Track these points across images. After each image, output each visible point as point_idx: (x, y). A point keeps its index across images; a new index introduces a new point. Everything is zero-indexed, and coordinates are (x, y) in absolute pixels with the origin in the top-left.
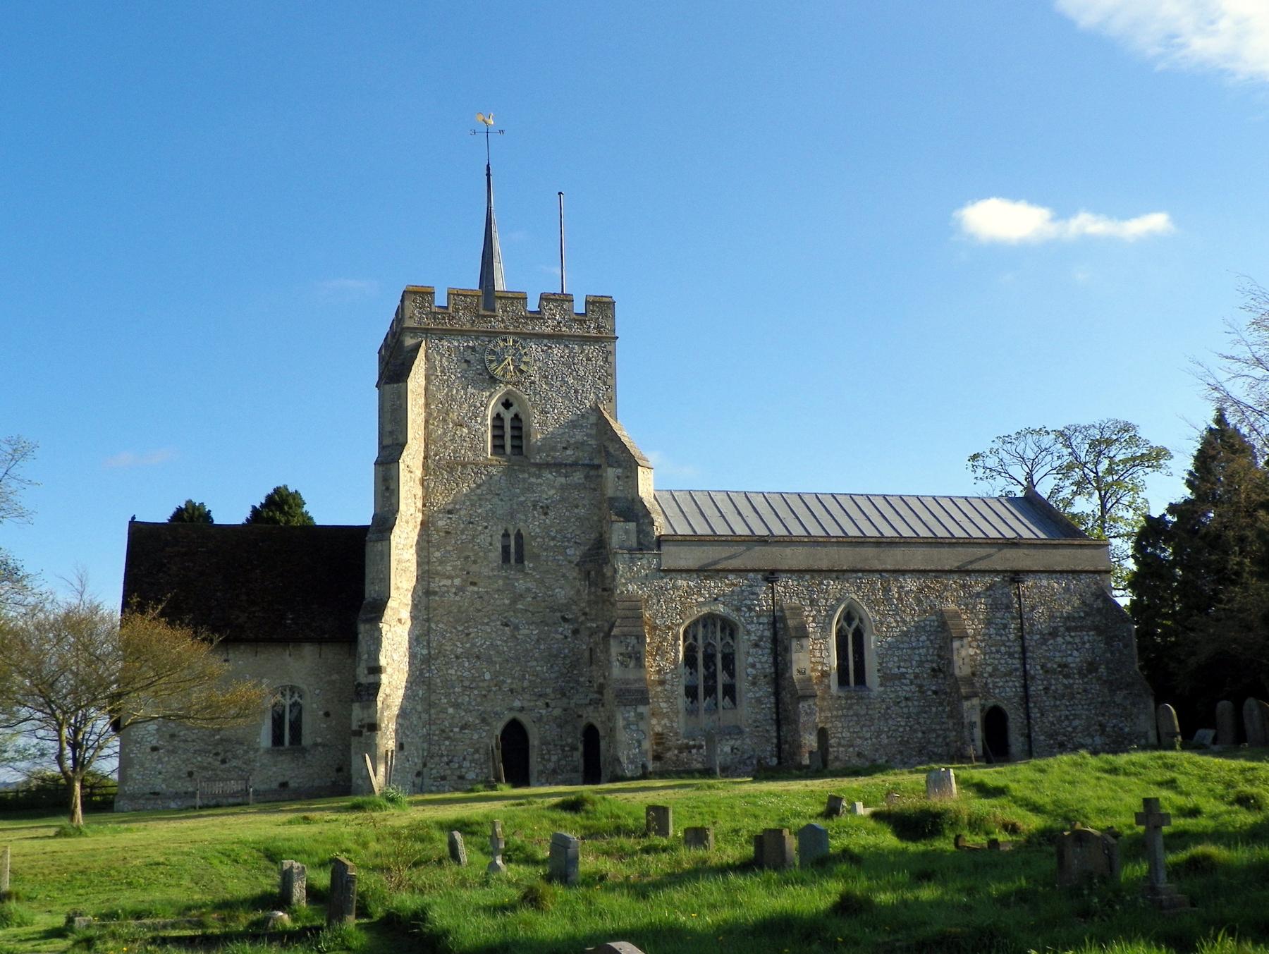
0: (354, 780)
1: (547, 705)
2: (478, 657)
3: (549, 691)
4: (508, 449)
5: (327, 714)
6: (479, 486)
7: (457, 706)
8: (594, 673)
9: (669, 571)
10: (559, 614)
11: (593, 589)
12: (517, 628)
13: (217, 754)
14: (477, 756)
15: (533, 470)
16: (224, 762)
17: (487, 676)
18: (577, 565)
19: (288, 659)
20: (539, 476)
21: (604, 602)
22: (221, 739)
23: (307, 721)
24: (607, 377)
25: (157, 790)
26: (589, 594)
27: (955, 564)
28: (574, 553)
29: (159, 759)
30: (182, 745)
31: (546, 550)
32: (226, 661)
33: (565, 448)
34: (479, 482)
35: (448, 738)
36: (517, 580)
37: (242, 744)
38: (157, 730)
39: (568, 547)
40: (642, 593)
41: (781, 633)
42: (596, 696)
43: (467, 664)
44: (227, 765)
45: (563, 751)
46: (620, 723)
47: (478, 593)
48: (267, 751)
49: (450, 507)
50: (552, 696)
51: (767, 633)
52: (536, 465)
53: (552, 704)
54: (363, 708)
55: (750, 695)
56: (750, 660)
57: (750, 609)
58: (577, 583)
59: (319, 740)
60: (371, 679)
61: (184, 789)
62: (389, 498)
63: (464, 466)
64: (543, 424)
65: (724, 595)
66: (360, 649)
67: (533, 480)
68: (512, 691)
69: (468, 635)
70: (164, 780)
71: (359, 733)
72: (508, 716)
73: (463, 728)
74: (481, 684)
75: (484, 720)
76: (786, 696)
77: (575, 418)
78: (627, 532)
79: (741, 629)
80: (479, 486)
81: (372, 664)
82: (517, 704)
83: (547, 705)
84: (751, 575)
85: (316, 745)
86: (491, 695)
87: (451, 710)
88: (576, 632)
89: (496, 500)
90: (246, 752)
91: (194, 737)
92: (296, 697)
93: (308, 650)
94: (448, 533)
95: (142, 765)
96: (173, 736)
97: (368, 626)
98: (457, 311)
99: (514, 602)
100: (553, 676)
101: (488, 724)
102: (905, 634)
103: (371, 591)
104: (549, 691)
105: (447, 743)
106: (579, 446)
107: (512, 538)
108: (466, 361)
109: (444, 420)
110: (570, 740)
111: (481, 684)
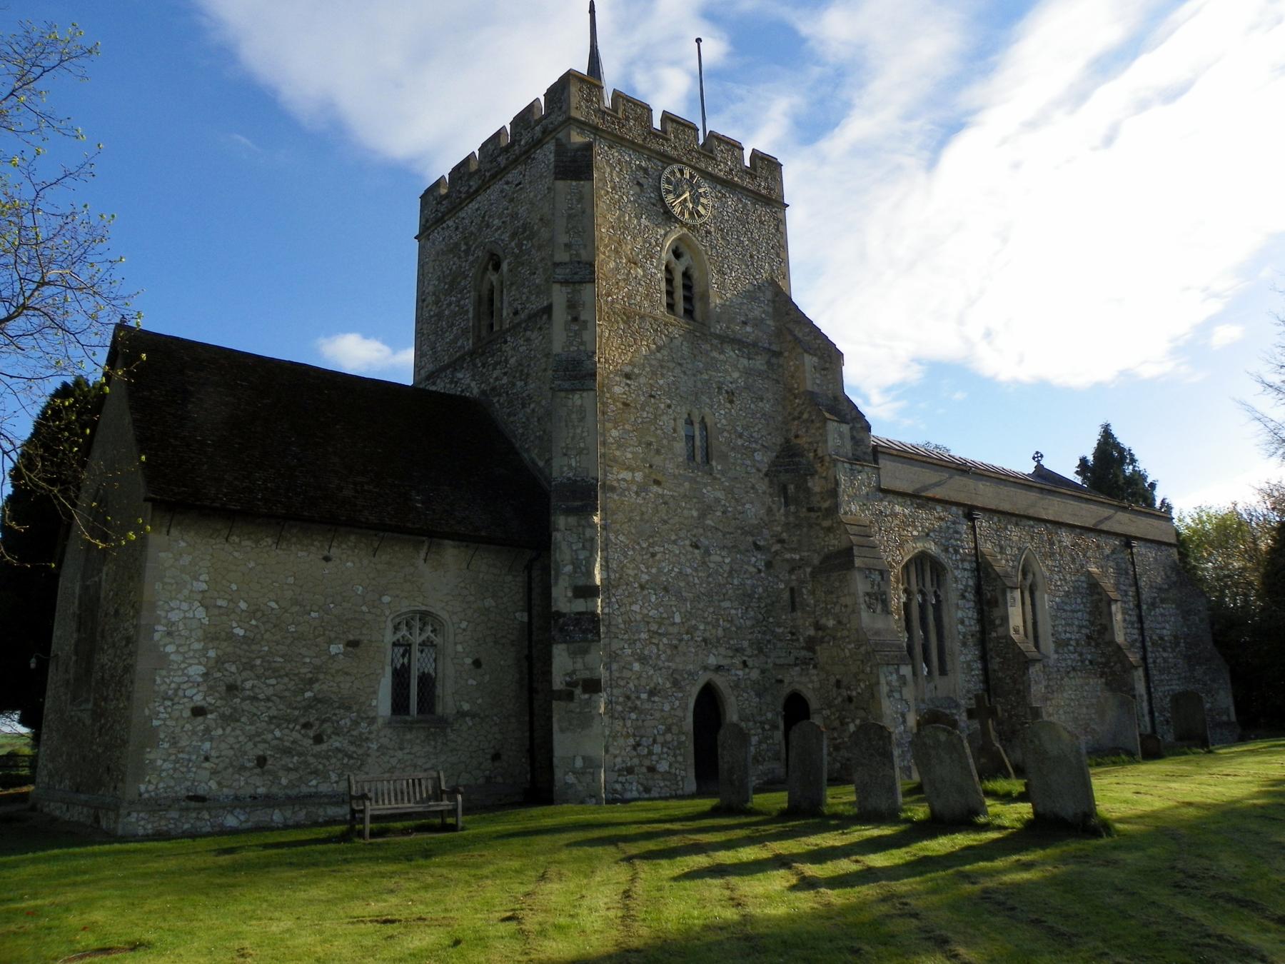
0: (558, 774)
1: (745, 664)
2: (666, 589)
3: (745, 644)
5: (477, 663)
6: (659, 349)
7: (643, 659)
8: (800, 622)
9: (886, 492)
10: (750, 539)
11: (792, 508)
12: (707, 552)
13: (307, 726)
14: (669, 737)
15: (715, 342)
16: (318, 739)
17: (677, 619)
18: (766, 475)
20: (722, 352)
21: (810, 526)
22: (315, 698)
25: (201, 792)
26: (786, 515)
27: (1089, 523)
28: (763, 459)
29: (207, 730)
30: (246, 705)
31: (733, 449)
32: (327, 559)
33: (745, 323)
34: (660, 343)
35: (634, 709)
36: (705, 485)
37: (349, 708)
38: (205, 675)
39: (755, 450)
40: (866, 517)
41: (987, 589)
42: (804, 653)
43: (653, 598)
44: (324, 747)
45: (763, 729)
46: (884, 689)
47: (663, 496)
48: (389, 724)
49: (628, 369)
50: (749, 652)
51: (971, 583)
52: (718, 337)
53: (750, 663)
54: (573, 654)
55: (962, 658)
56: (960, 614)
57: (956, 552)
58: (768, 500)
59: (466, 707)
60: (580, 606)
61: (250, 791)
62: (578, 334)
63: (642, 317)
64: (722, 286)
65: (934, 531)
66: (557, 556)
67: (715, 354)
68: (705, 640)
69: (653, 555)
70: (214, 772)
71: (569, 696)
72: (703, 679)
73: (652, 693)
74: (671, 629)
75: (676, 683)
76: (995, 663)
77: (751, 288)
78: (841, 435)
79: (949, 576)
80: (659, 349)
81: (581, 582)
82: (712, 660)
83: (745, 664)
84: (954, 509)
85: (462, 714)
86: (682, 647)
87: (637, 666)
88: (769, 565)
89: (678, 371)
90: (356, 723)
91: (270, 691)
92: (428, 632)
93: (451, 554)
94: (626, 405)
95: (174, 743)
96: (232, 688)
97: (572, 520)
98: (627, 119)
99: (703, 516)
100: (749, 623)
101: (681, 689)
102: (1067, 594)
104: (745, 644)
105: (633, 716)
106: (758, 323)
107: (697, 426)
108: (639, 184)
109: (617, 251)
110: (769, 715)
111: (671, 629)
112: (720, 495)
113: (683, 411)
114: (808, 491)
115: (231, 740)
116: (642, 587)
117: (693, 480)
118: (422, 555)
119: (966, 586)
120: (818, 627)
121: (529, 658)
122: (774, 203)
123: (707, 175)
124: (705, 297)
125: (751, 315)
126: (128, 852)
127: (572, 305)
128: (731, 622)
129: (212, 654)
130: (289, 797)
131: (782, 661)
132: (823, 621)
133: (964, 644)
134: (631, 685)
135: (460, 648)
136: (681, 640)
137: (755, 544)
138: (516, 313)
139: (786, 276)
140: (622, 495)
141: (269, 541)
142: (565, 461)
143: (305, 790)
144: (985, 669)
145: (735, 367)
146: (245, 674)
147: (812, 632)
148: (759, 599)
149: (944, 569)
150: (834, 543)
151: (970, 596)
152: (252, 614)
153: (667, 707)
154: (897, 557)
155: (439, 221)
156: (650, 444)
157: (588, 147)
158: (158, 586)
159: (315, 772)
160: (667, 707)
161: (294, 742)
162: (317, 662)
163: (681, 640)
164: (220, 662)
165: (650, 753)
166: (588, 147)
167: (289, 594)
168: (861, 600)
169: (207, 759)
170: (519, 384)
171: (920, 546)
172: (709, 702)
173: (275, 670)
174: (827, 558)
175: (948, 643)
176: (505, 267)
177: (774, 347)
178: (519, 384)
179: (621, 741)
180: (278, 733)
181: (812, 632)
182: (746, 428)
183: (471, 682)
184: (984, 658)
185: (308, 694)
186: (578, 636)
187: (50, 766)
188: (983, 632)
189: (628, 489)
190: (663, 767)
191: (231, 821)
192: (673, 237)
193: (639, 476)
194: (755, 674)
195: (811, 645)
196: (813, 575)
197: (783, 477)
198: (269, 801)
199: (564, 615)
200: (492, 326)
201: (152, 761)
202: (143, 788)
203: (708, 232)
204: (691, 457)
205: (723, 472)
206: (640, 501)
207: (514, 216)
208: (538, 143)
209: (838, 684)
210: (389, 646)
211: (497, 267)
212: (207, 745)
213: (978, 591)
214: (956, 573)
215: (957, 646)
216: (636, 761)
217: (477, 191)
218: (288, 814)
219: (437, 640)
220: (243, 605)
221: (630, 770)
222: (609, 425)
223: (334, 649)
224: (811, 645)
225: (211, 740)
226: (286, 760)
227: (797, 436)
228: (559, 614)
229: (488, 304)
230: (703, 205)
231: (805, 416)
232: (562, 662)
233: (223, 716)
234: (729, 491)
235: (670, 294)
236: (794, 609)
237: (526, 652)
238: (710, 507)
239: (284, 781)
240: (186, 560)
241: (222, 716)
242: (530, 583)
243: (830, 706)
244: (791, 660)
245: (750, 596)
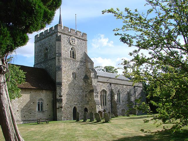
0: (58, 117)
4: (72, 57)
5: (47, 105)
9: (99, 82)
16: (30, 114)
19: (41, 93)
23: (44, 105)
24: (86, 47)
28: (83, 77)
41: (112, 95)
46: (97, 108)
48: (38, 112)
60: (60, 98)
71: (59, 109)
75: (71, 107)
76: (113, 104)
82: (75, 104)
88: (83, 91)
93: (44, 91)
103: (57, 81)
113: (72, 71)
120: (89, 99)
121: (53, 104)
123: (76, 37)
124: (75, 55)
127: (58, 59)
142: (58, 80)
143: (29, 119)
150: (91, 89)
154: (99, 90)
155: (38, 41)
157: (60, 36)
159: (30, 117)
166: (60, 36)
171: (103, 89)
172: (75, 109)
174: (91, 90)
176: (48, 50)
177: (85, 62)
184: (111, 103)
188: (111, 100)
190: (69, 117)
192: (71, 47)
194: (81, 105)
195: (88, 102)
200: (46, 58)
203: (76, 46)
207: (50, 44)
208: (53, 34)
211: (47, 50)
213: (111, 94)
217: (44, 38)
219: (43, 102)
223: (31, 103)
224: (88, 102)
226: (27, 116)
229: (46, 55)
232: (58, 105)
235: (71, 55)
242: (53, 95)
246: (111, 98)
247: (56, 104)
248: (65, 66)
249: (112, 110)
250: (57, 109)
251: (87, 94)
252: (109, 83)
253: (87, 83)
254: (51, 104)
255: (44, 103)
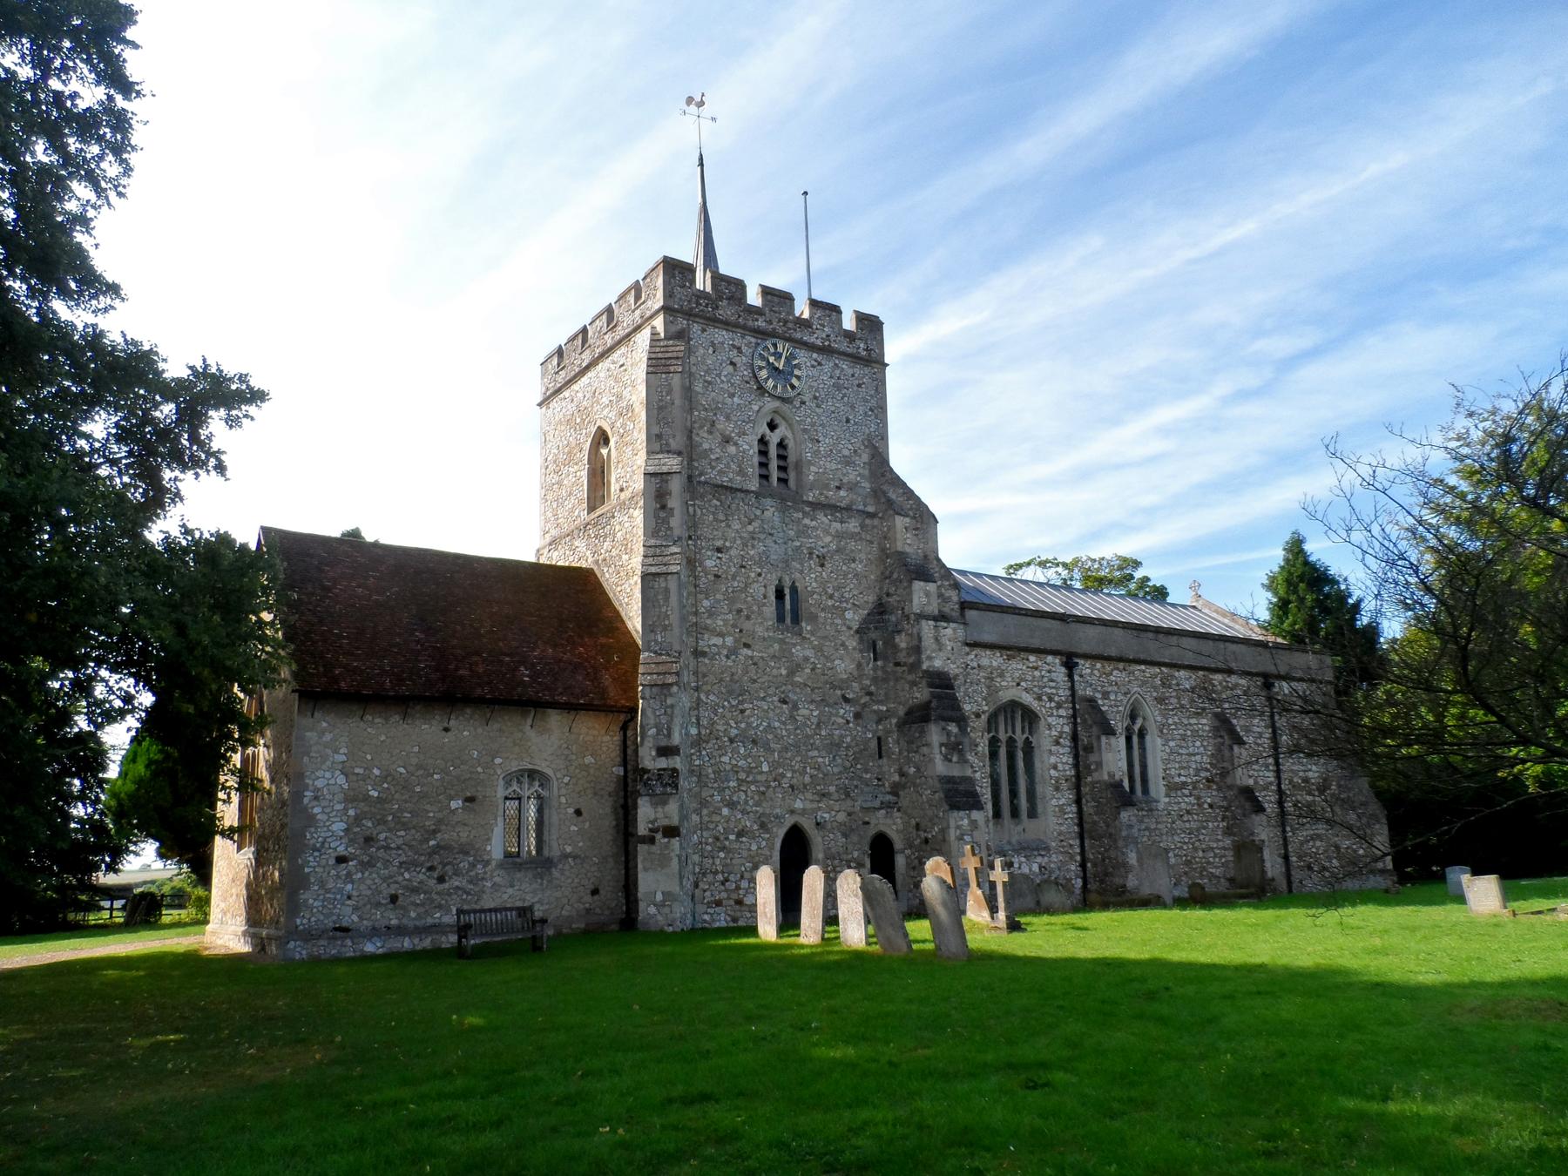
0: (642, 905)
2: (754, 742)
3: (832, 789)
5: (578, 812)
7: (732, 805)
8: (885, 769)
10: (839, 692)
11: (879, 663)
12: (795, 707)
13: (431, 869)
16: (441, 880)
17: (765, 768)
18: (857, 632)
19: (531, 733)
21: (897, 680)
22: (438, 846)
25: (345, 924)
26: (875, 669)
28: (854, 617)
29: (349, 875)
30: (381, 853)
32: (446, 730)
33: (839, 488)
35: (723, 848)
36: (795, 645)
37: (467, 853)
38: (346, 830)
42: (889, 798)
44: (446, 885)
48: (501, 866)
50: (836, 796)
51: (1067, 729)
52: (810, 504)
55: (1054, 802)
56: (1053, 760)
58: (858, 656)
59: (569, 849)
60: (663, 763)
61: (385, 922)
67: (807, 521)
69: (742, 711)
70: (356, 909)
71: (652, 841)
72: (789, 821)
73: (740, 834)
74: (759, 777)
75: (763, 826)
76: (1088, 808)
78: (927, 594)
81: (664, 743)
84: (1050, 658)
85: (565, 856)
86: (770, 793)
87: (725, 811)
88: (857, 716)
90: (473, 866)
91: (400, 842)
93: (555, 719)
94: (717, 576)
95: (322, 884)
96: (369, 840)
99: (791, 673)
100: (836, 770)
101: (767, 831)
104: (832, 789)
105: (722, 855)
106: (852, 487)
110: (856, 854)
111: (759, 777)
112: (809, 653)
114: (895, 646)
115: (369, 882)
116: (731, 741)
117: (782, 642)
118: (529, 721)
119: (1061, 733)
122: (874, 362)
125: (845, 480)
126: (540, 823)
128: (818, 769)
129: (351, 812)
130: (416, 928)
131: (869, 805)
132: (905, 769)
133: (1057, 789)
134: (720, 828)
135: (563, 800)
136: (768, 787)
137: (844, 697)
138: (622, 490)
139: (884, 437)
140: (712, 659)
141: (397, 717)
143: (430, 921)
144: (1080, 812)
145: (827, 533)
146: (380, 828)
147: (896, 778)
148: (847, 748)
149: (1037, 716)
151: (1066, 742)
152: (384, 778)
153: (754, 847)
156: (739, 611)
158: (306, 759)
159: (440, 907)
160: (754, 847)
161: (421, 882)
162: (439, 815)
163: (768, 787)
164: (358, 820)
165: (738, 888)
167: (414, 761)
168: (936, 750)
169: (349, 898)
170: (625, 557)
173: (404, 824)
175: (1039, 789)
177: (871, 509)
178: (625, 557)
179: (710, 877)
180: (407, 875)
181: (896, 778)
182: (837, 589)
183: (574, 828)
184: (1078, 802)
185: (432, 843)
186: (659, 790)
187: (223, 905)
188: (1078, 777)
189: (719, 654)
191: (369, 948)
193: (729, 641)
194: (841, 817)
195: (895, 790)
196: (900, 726)
197: (873, 635)
198: (401, 931)
199: (648, 771)
201: (306, 901)
202: (298, 921)
203: (803, 403)
204: (781, 618)
205: (812, 633)
206: (730, 663)
207: (619, 397)
209: (918, 827)
210: (501, 801)
212: (349, 887)
214: (1050, 720)
215: (1049, 790)
216: (724, 895)
218: (416, 941)
220: (377, 772)
221: (718, 903)
222: (700, 596)
223: (454, 805)
225: (352, 882)
227: (888, 595)
228: (645, 771)
230: (798, 378)
231: (895, 576)
232: (646, 813)
233: (361, 863)
234: (819, 649)
235: (763, 465)
236: (880, 757)
237: (622, 801)
238: (798, 665)
239: (413, 914)
240: (328, 737)
241: (361, 863)
243: (911, 847)
244: (877, 804)
245: (838, 746)
246: (1076, 765)
247: (635, 807)
248: (719, 543)
249: (1083, 853)
250: (218, 838)
251: (888, 732)
252: (1054, 653)
253: (885, 658)
254: (608, 810)
255: (555, 803)
